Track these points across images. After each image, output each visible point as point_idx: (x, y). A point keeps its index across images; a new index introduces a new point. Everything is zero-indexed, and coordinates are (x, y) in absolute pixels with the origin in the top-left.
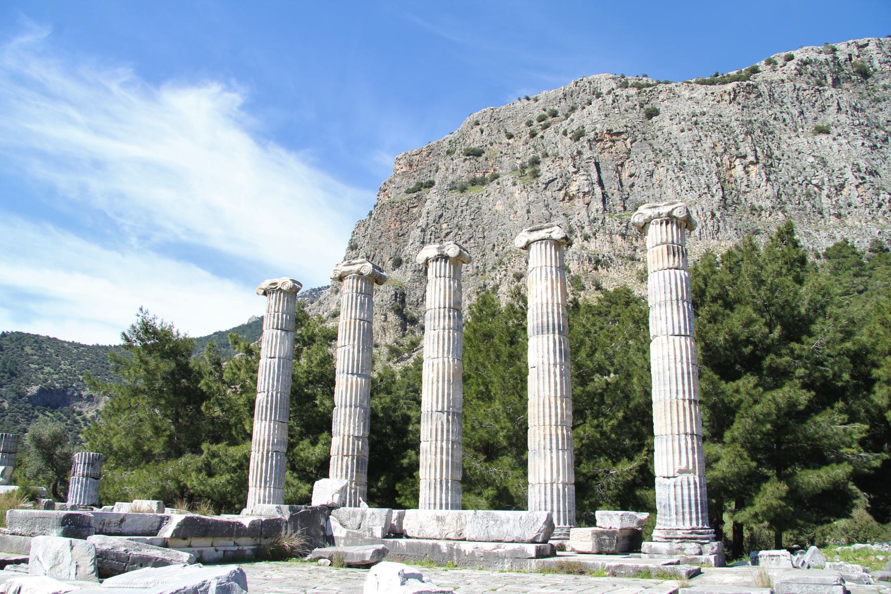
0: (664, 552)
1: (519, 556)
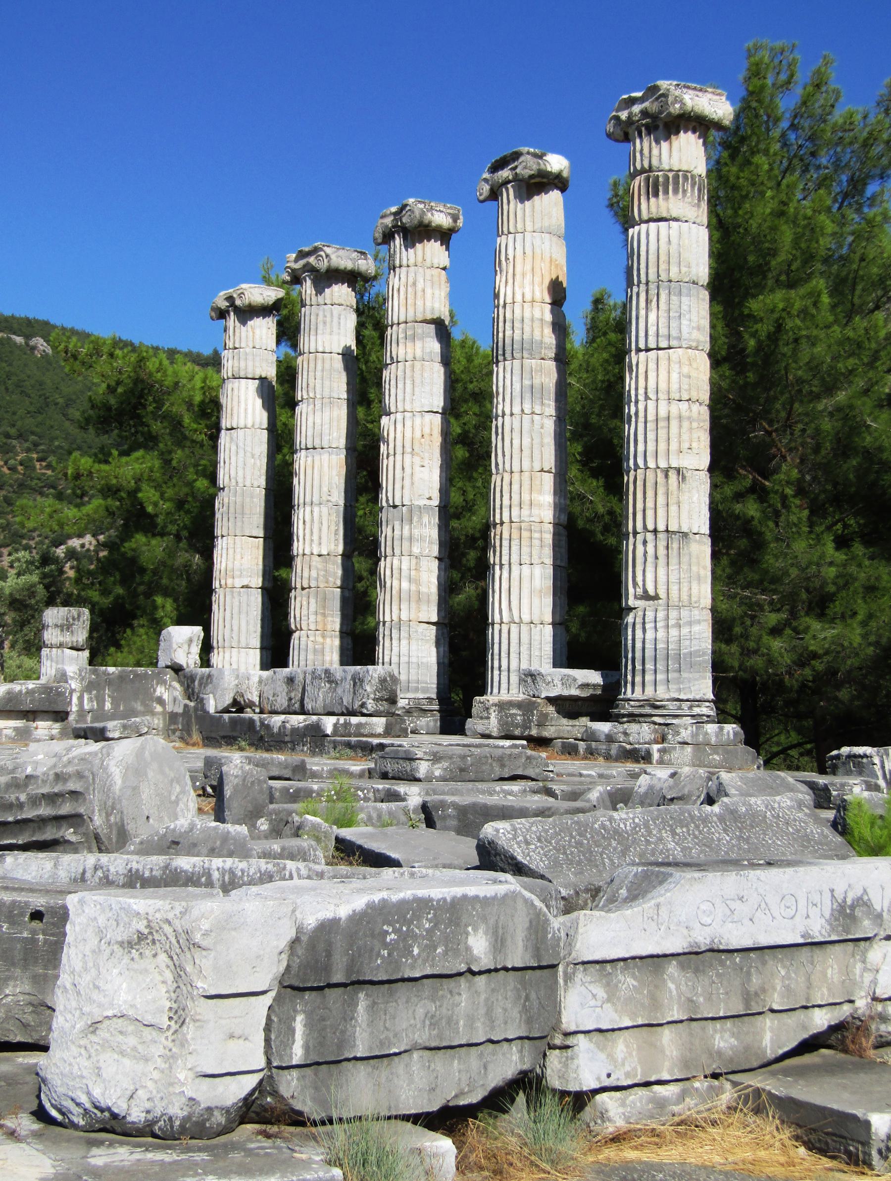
0: (602, 738)
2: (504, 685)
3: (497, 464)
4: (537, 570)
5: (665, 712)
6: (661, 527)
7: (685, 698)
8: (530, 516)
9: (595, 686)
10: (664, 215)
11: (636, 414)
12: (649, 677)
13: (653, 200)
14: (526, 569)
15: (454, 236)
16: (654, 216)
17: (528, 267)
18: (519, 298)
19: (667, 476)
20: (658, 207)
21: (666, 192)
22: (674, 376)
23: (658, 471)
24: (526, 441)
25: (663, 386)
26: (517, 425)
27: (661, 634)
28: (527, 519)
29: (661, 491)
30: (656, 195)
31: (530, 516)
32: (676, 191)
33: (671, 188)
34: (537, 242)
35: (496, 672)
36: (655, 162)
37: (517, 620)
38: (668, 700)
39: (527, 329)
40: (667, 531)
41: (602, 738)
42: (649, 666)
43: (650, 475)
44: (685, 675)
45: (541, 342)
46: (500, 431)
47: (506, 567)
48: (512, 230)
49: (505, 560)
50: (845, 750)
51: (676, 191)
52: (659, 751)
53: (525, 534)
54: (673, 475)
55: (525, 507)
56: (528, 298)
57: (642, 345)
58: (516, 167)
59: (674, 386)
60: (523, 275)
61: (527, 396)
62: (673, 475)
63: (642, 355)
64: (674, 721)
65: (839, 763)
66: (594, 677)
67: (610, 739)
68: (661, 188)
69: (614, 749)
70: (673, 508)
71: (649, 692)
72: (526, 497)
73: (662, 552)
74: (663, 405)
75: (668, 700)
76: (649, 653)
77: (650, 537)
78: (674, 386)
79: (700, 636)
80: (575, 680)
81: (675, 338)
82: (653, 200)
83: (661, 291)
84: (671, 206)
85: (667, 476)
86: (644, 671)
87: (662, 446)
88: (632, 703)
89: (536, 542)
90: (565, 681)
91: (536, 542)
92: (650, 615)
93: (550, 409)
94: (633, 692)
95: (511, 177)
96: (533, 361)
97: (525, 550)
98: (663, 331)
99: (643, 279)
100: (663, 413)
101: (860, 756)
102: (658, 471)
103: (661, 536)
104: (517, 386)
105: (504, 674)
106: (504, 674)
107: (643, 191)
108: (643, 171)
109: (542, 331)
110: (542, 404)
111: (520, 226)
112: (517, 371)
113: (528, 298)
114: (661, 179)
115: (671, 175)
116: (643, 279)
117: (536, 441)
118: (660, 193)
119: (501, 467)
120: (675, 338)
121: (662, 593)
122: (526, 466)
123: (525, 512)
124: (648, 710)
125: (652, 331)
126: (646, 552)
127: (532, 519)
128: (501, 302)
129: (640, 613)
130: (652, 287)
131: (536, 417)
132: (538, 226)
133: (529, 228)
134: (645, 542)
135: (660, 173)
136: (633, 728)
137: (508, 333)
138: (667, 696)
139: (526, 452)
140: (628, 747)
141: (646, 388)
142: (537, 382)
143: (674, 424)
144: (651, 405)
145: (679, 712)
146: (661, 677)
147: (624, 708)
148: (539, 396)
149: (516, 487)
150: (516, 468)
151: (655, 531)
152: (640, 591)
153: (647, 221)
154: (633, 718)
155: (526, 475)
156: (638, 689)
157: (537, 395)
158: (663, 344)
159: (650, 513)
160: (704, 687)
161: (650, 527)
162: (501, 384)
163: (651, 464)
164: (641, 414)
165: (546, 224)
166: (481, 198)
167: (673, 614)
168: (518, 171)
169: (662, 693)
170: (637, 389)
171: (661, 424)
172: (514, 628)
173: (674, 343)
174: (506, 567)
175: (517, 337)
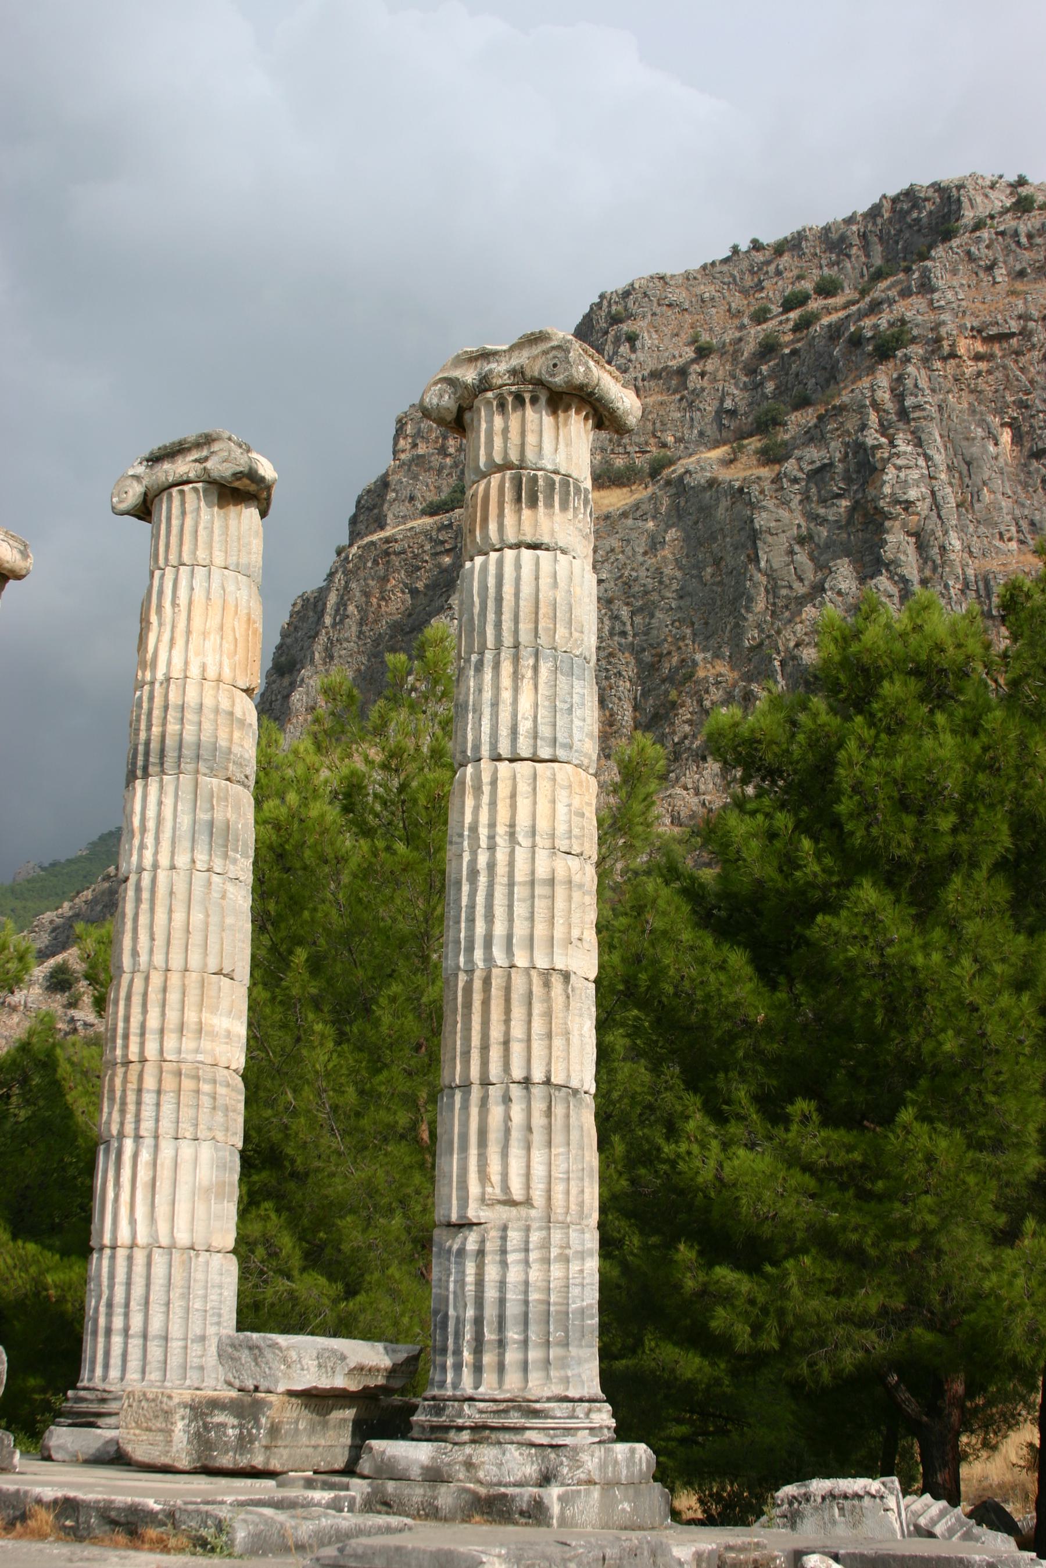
0: (415, 1472)
2: (134, 1363)
3: (135, 953)
4: (206, 1151)
5: (550, 1423)
6: (538, 1076)
7: (577, 1396)
8: (197, 1051)
9: (372, 1371)
10: (546, 540)
11: (491, 866)
12: (512, 1356)
13: (526, 513)
14: (186, 1150)
15: (11, 584)
16: (529, 539)
17: (214, 622)
18: (194, 671)
19: (547, 985)
20: (536, 524)
21: (549, 505)
22: (561, 810)
23: (534, 973)
24: (197, 917)
25: (542, 825)
26: (180, 888)
27: (535, 1274)
28: (190, 1057)
29: (538, 1008)
30: (533, 503)
31: (197, 1051)
32: (564, 507)
33: (557, 498)
34: (231, 588)
35: (117, 1340)
36: (530, 455)
37: (164, 1241)
38: (549, 1400)
39: (207, 726)
40: (548, 1082)
41: (415, 1472)
42: (513, 1334)
43: (518, 982)
44: (573, 1351)
45: (229, 751)
46: (145, 895)
47: (148, 1142)
48: (186, 558)
49: (147, 1126)
50: (819, 1486)
51: (564, 507)
52: (560, 1498)
53: (187, 1084)
54: (556, 981)
55: (189, 1034)
56: (211, 674)
57: (504, 750)
58: (206, 459)
59: (561, 828)
60: (205, 634)
61: (203, 838)
62: (556, 981)
63: (503, 767)
64: (567, 1440)
65: (807, 1508)
66: (372, 1356)
67: (434, 1476)
68: (541, 496)
69: (445, 1497)
70: (558, 1042)
71: (513, 1381)
72: (191, 1017)
73: (538, 1120)
74: (542, 855)
75: (549, 1400)
76: (513, 1309)
77: (516, 1091)
78: (561, 828)
79: (576, 1274)
80: (343, 1358)
81: (564, 746)
82: (526, 513)
83: (541, 662)
84: (557, 528)
85: (547, 985)
86: (501, 1344)
87: (540, 929)
88: (481, 1405)
89: (206, 1101)
90: (323, 1360)
91: (206, 1101)
92: (514, 1237)
93: (243, 868)
94: (501, 1381)
95: (192, 475)
96: (214, 780)
97: (186, 1113)
98: (545, 731)
99: (508, 640)
100: (542, 871)
101: (858, 1496)
102: (534, 973)
103: (537, 1091)
104: (185, 820)
105: (135, 1343)
106: (135, 1343)
107: (508, 496)
108: (507, 466)
109: (231, 733)
110: (226, 856)
111: (202, 555)
112: (186, 794)
113: (211, 674)
114: (541, 482)
115: (557, 478)
116: (508, 640)
117: (214, 919)
118: (541, 504)
119: (143, 959)
120: (564, 746)
121: (538, 1195)
122: (195, 960)
123: (188, 1044)
124: (515, 1419)
125: (525, 726)
126: (508, 1118)
127: (200, 1057)
128: (160, 675)
129: (494, 1234)
130: (526, 653)
131: (216, 879)
132: (232, 560)
133: (219, 559)
134: (507, 1100)
135: (540, 473)
136: (486, 1455)
137: (172, 728)
138: (547, 1393)
139: (196, 938)
140: (482, 1491)
141: (512, 825)
142: (219, 816)
143: (560, 891)
144: (521, 855)
145: (571, 1423)
146: (534, 1355)
147: (460, 1414)
148: (220, 841)
149: (173, 997)
150: (176, 962)
151: (527, 1082)
152: (495, 1191)
153: (517, 546)
154: (480, 1432)
155: (193, 977)
156: (489, 1378)
157: (218, 840)
158: (544, 753)
159: (517, 1049)
160: (586, 1374)
161: (517, 1073)
162: (151, 813)
163: (521, 960)
164: (501, 869)
165: (244, 560)
166: (123, 506)
167: (557, 1236)
168: (209, 465)
169: (538, 1386)
170: (492, 825)
171: (539, 890)
172: (158, 1258)
173: (561, 753)
174: (148, 1142)
175: (189, 737)
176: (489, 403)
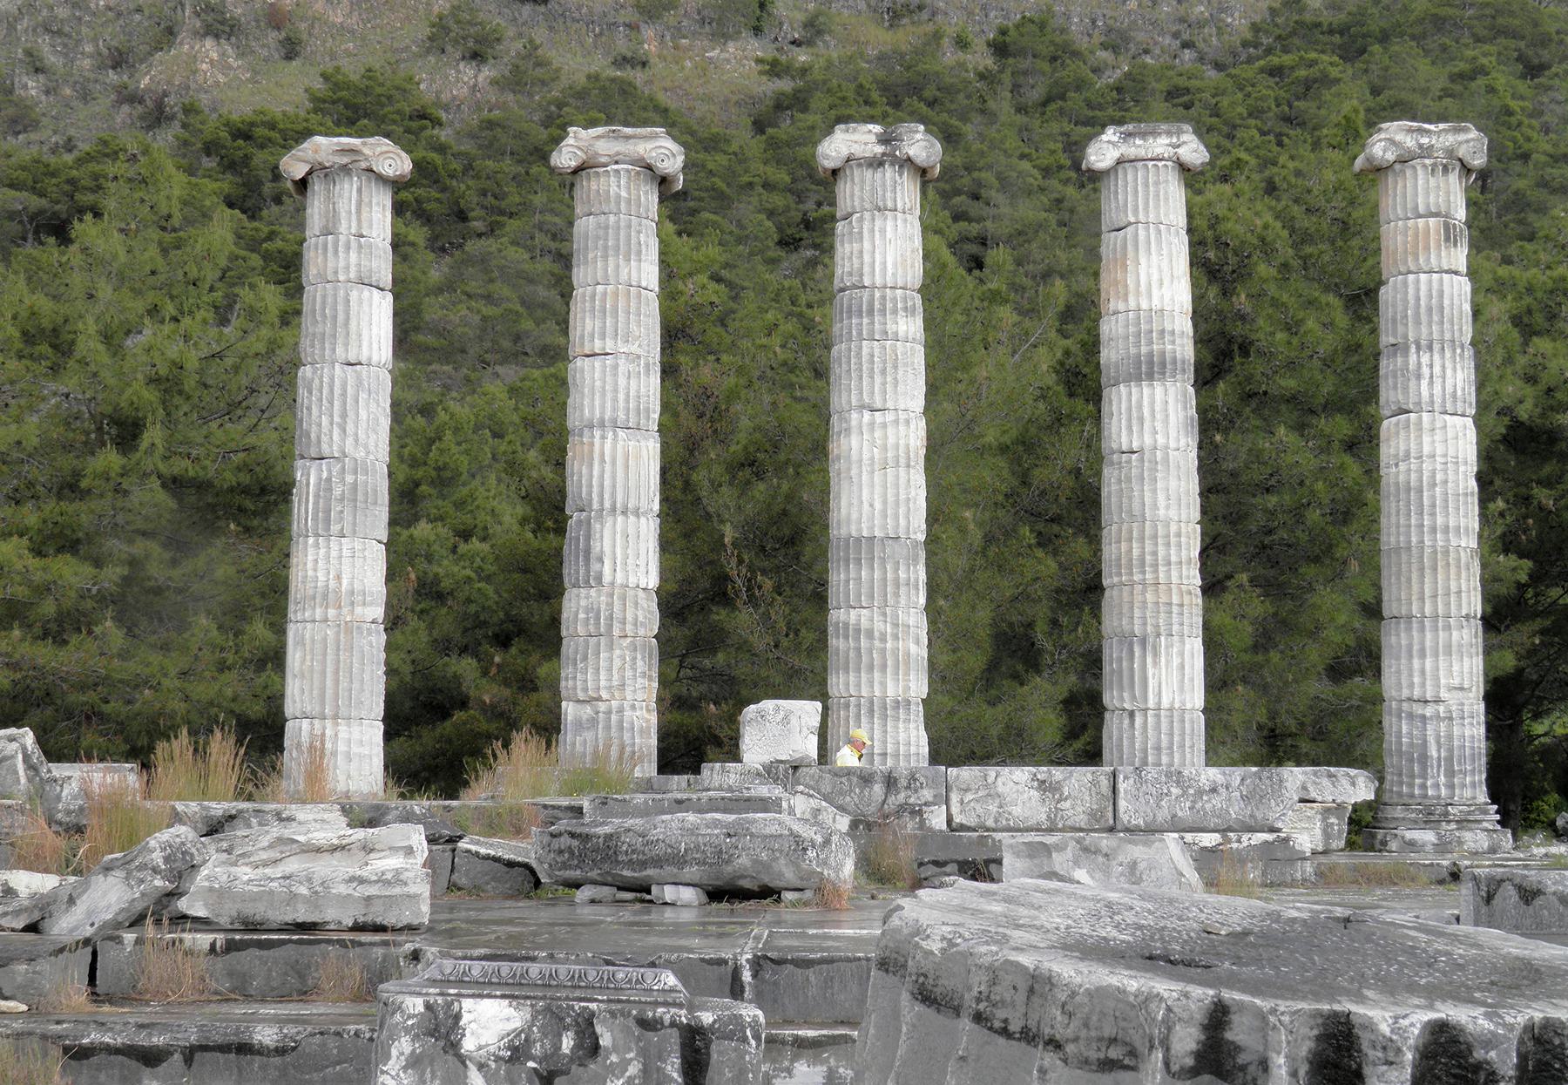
1: (1279, 855)
136: (1467, 835)
168: (1180, 151)
176: (1424, 166)
